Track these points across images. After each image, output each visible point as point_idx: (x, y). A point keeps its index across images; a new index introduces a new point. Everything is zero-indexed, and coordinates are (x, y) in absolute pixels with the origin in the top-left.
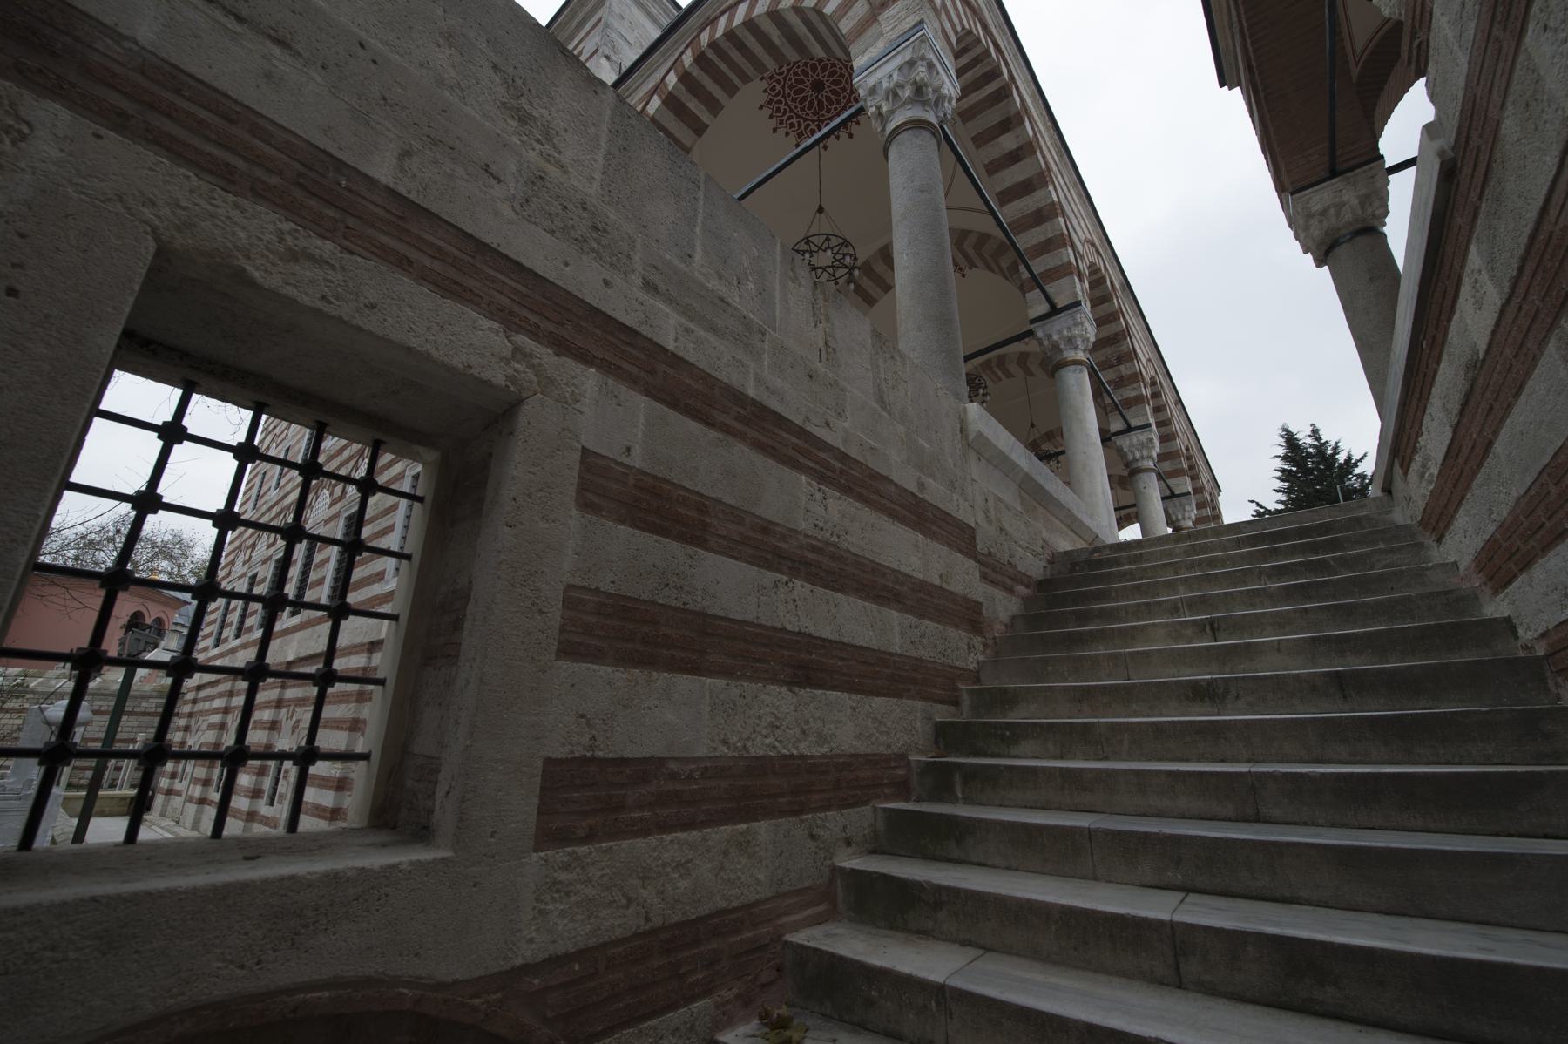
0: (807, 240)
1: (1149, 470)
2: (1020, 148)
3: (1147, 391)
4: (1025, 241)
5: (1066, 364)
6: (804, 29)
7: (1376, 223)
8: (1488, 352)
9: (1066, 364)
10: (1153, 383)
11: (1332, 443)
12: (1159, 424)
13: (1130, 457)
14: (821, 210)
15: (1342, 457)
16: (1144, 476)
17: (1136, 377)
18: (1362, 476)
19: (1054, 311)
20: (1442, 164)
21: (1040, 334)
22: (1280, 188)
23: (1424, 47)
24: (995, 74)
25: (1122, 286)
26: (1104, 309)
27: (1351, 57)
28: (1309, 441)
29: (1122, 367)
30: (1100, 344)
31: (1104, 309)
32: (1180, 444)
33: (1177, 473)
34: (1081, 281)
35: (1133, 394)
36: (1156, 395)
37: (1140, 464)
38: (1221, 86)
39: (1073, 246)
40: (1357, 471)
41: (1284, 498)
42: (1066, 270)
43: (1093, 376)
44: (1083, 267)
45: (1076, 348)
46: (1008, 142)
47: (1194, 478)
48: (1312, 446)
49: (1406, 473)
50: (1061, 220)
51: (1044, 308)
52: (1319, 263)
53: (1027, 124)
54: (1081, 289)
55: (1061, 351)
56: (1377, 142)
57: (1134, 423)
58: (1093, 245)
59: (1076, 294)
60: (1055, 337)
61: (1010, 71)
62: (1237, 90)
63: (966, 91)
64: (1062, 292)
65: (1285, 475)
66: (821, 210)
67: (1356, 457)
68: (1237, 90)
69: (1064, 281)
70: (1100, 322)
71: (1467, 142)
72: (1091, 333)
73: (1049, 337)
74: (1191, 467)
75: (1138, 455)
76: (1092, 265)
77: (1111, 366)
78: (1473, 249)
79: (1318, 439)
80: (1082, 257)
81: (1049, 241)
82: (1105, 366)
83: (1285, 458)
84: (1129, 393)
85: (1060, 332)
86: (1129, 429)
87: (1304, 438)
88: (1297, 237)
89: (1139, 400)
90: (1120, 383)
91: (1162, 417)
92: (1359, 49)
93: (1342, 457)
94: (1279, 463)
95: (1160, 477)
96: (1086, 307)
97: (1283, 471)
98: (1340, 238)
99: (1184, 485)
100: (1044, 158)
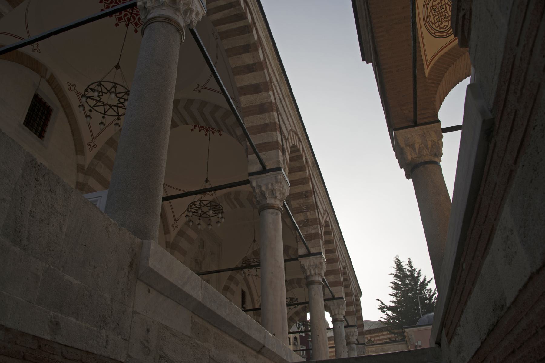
0: (100, 84)
1: (318, 283)
2: (254, 64)
3: (321, 231)
4: (248, 122)
5: (268, 207)
6: (226, 12)
7: (436, 159)
8: (514, 303)
9: (268, 207)
10: (327, 225)
11: (417, 270)
12: (327, 252)
13: (308, 273)
14: (117, 67)
15: (421, 279)
16: (315, 287)
17: (316, 221)
18: (430, 291)
19: (264, 170)
20: (484, 121)
21: (254, 184)
22: (393, 126)
23: (467, 17)
24: (243, 17)
25: (313, 162)
26: (298, 175)
27: (424, 62)
28: (407, 267)
29: (308, 213)
30: (291, 197)
31: (298, 175)
32: (339, 266)
33: (336, 284)
34: (284, 154)
35: (314, 232)
36: (328, 233)
37: (311, 279)
38: (363, 60)
39: (281, 131)
40: (428, 287)
41: (395, 299)
42: (274, 146)
43: (286, 215)
44: (287, 146)
45: (275, 197)
46: (247, 59)
47: (346, 286)
48: (408, 270)
49: (449, 342)
50: (275, 114)
51: (258, 167)
52: (408, 177)
53: (260, 52)
54: (283, 160)
55: (266, 198)
56: (437, 117)
57: (313, 251)
58: (297, 134)
59: (279, 162)
60: (263, 188)
61: (253, 19)
62: (371, 64)
63: (210, 12)
64: (270, 158)
65: (396, 287)
66: (117, 67)
67: (428, 280)
68: (371, 64)
69: (272, 153)
70: (293, 183)
71: (505, 106)
72: (287, 188)
73: (260, 187)
74: (345, 280)
75: (313, 273)
76: (293, 147)
77: (302, 212)
78: (506, 209)
79: (411, 267)
80: (287, 140)
81: (266, 125)
82: (296, 211)
83: (396, 276)
84: (311, 231)
85: (267, 185)
86: (309, 254)
87: (406, 267)
88: (397, 157)
89: (317, 236)
90: (306, 223)
91: (330, 247)
92: (429, 59)
93: (421, 279)
94: (392, 279)
95: (325, 286)
96: (284, 172)
97: (395, 283)
98: (419, 166)
99: (340, 292)
100: (269, 74)
